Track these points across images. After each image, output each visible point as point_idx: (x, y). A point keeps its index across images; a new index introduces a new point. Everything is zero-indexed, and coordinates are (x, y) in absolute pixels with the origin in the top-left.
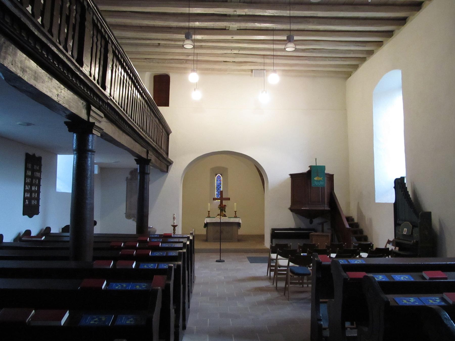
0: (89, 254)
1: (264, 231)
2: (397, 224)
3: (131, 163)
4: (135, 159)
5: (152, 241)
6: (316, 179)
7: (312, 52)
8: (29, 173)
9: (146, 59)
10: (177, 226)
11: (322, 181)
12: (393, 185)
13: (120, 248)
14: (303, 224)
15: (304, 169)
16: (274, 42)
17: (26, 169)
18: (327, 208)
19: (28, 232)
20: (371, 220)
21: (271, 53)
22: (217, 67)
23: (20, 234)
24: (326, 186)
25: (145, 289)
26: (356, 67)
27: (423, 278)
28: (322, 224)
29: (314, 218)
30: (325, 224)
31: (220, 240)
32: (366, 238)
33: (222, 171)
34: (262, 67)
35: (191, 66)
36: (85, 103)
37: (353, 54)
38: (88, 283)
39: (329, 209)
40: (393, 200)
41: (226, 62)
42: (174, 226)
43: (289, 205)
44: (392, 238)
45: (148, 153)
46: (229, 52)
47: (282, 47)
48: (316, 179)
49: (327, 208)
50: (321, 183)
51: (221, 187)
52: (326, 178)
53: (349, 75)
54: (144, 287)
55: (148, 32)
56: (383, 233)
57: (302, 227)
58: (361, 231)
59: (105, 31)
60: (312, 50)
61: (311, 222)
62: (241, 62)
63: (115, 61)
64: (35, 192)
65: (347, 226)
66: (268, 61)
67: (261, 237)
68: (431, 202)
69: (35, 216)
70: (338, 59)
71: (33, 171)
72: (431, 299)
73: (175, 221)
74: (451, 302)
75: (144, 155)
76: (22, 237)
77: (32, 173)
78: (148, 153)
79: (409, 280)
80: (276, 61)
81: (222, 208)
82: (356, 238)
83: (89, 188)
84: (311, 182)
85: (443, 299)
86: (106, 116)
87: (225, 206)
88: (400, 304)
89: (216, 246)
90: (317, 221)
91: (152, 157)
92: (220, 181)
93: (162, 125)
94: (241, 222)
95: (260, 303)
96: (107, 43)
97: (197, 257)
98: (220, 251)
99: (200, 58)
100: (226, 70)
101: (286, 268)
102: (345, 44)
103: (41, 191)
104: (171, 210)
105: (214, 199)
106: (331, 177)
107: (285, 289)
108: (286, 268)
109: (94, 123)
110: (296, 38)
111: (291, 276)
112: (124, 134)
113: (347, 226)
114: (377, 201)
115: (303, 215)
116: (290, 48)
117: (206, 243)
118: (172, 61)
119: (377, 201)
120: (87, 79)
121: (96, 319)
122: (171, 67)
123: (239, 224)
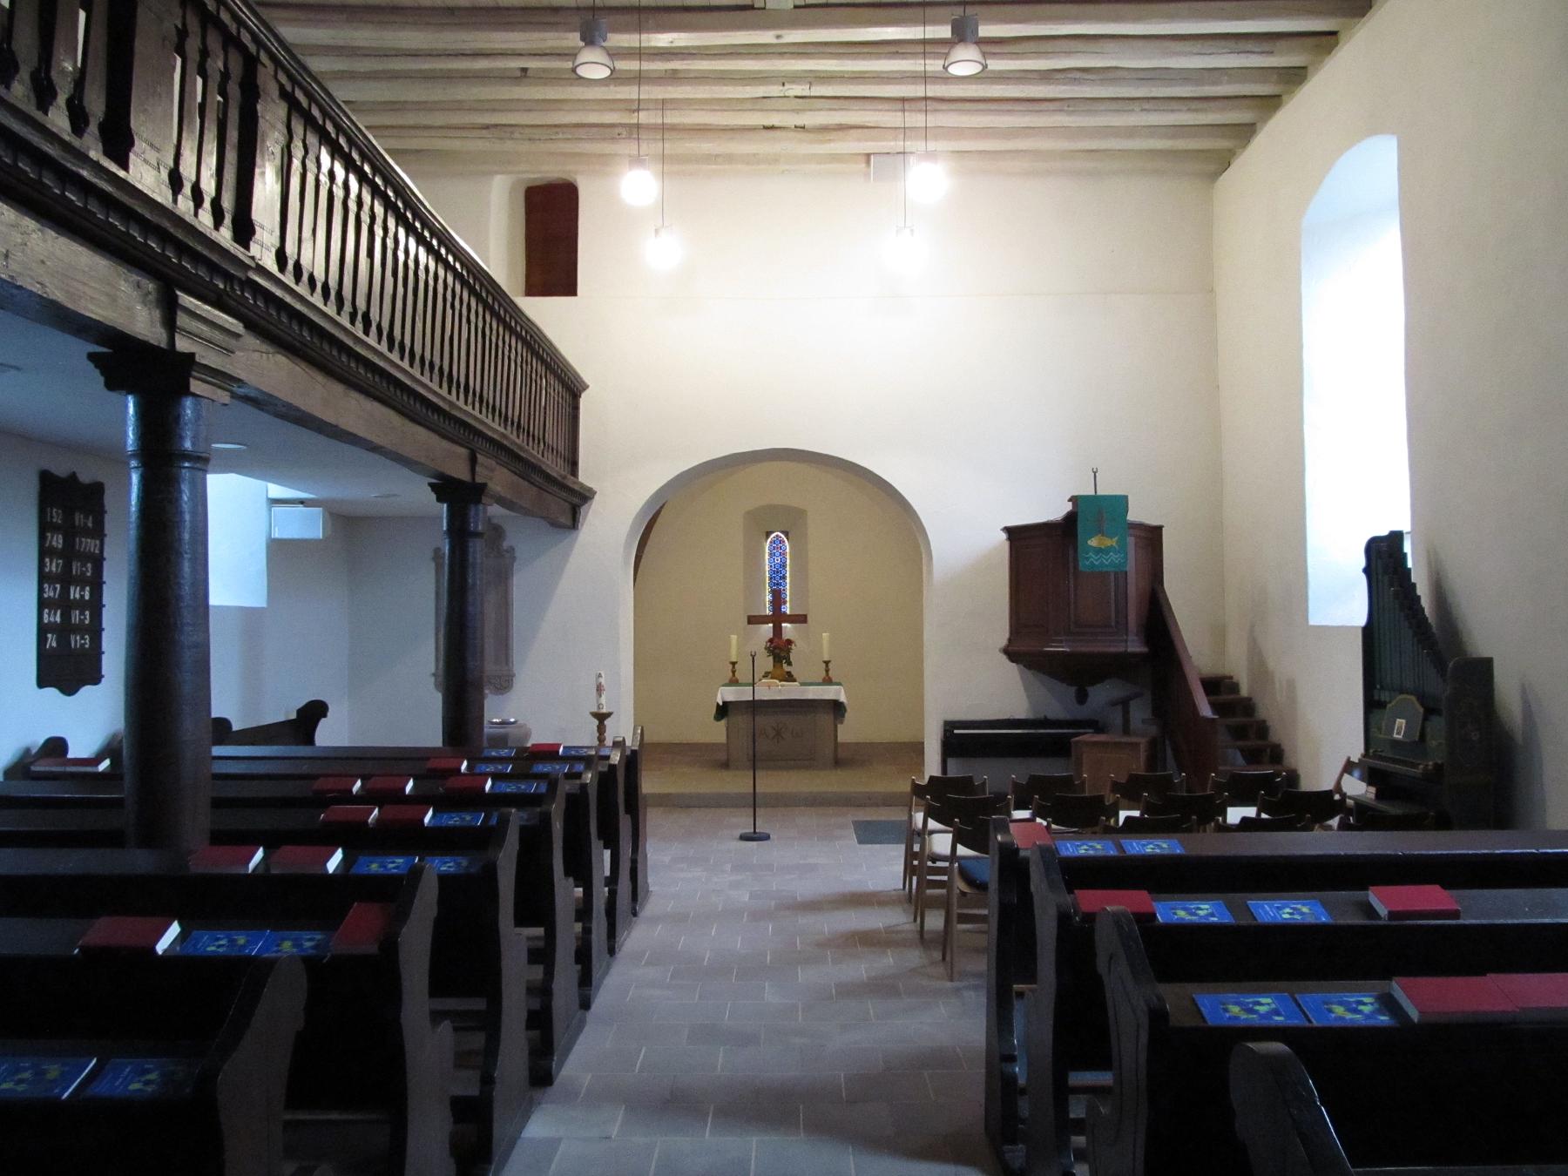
0: (195, 823)
1: (922, 730)
2: (1372, 705)
3: (418, 496)
4: (430, 485)
5: (477, 770)
6: (1093, 542)
7: (1075, 81)
8: (57, 541)
9: (487, 127)
10: (609, 715)
11: (1116, 552)
12: (1362, 563)
13: (346, 797)
14: (1055, 703)
15: (1053, 509)
16: (929, 48)
17: (44, 528)
18: (1135, 646)
19: (56, 747)
20: (1291, 685)
21: (917, 90)
22: (706, 146)
23: (27, 751)
24: (1131, 567)
25: (310, 952)
26: (1245, 133)
27: (1370, 911)
28: (1124, 703)
29: (1093, 684)
30: (1133, 705)
31: (755, 763)
32: (1277, 754)
33: (789, 521)
34: (898, 145)
35: (628, 148)
36: (151, 286)
37: (1229, 82)
38: (104, 931)
39: (1144, 649)
40: (1361, 618)
41: (772, 128)
42: (601, 717)
43: (1002, 635)
44: (1356, 751)
45: (473, 461)
46: (775, 90)
47: (934, 65)
48: (1093, 542)
49: (1135, 646)
50: (1114, 558)
51: (784, 578)
52: (1131, 541)
53: (1223, 161)
54: (308, 944)
55: (477, 26)
56: (1329, 735)
57: (1051, 716)
58: (1262, 729)
59: (235, 17)
60: (1078, 75)
61: (1082, 697)
62: (824, 129)
63: (298, 128)
64: (81, 605)
65: (1206, 710)
66: (916, 119)
67: (918, 749)
68: (1493, 627)
69: (87, 691)
70: (1174, 105)
71: (70, 533)
72: (1341, 1003)
73: (603, 700)
74: (1414, 1014)
75: (460, 472)
76: (32, 763)
77: (69, 542)
78: (473, 461)
79: (1311, 920)
80: (934, 120)
81: (780, 650)
82: (1242, 751)
83: (186, 590)
84: (1076, 551)
85: (1388, 1003)
86: (250, 326)
87: (789, 642)
88: (1211, 1021)
89: (737, 783)
90: (1102, 694)
91: (497, 478)
92: (783, 554)
93: (543, 361)
94: (843, 699)
95: (848, 991)
96: (251, 63)
97: (653, 820)
98: (754, 802)
99: (672, 118)
100: (774, 160)
101: (946, 864)
102: (1198, 46)
103: (105, 600)
104: (583, 662)
105: (754, 620)
106: (1151, 538)
107: (944, 941)
108: (946, 864)
109: (192, 355)
110: (985, 31)
111: (963, 894)
112: (354, 395)
113: (1206, 710)
114: (1312, 622)
115: (1053, 674)
116: (965, 62)
117: (725, 774)
118: (581, 133)
119: (1312, 622)
120: (132, 196)
121: (26, 1075)
122: (580, 155)
123: (837, 708)
